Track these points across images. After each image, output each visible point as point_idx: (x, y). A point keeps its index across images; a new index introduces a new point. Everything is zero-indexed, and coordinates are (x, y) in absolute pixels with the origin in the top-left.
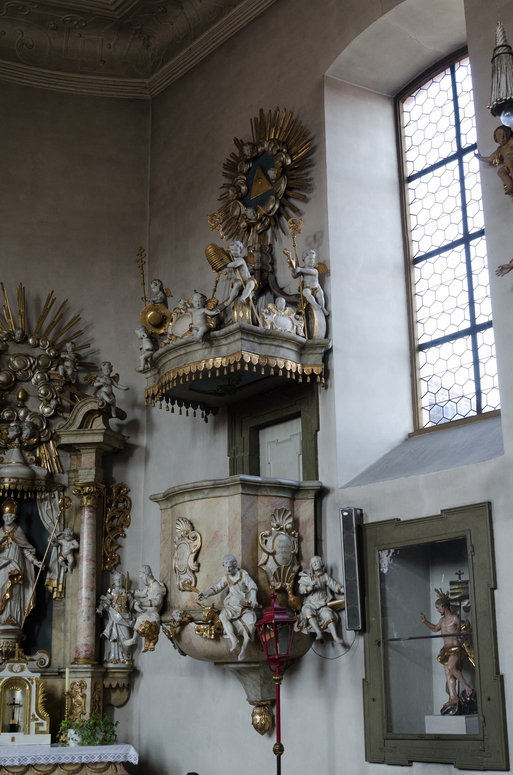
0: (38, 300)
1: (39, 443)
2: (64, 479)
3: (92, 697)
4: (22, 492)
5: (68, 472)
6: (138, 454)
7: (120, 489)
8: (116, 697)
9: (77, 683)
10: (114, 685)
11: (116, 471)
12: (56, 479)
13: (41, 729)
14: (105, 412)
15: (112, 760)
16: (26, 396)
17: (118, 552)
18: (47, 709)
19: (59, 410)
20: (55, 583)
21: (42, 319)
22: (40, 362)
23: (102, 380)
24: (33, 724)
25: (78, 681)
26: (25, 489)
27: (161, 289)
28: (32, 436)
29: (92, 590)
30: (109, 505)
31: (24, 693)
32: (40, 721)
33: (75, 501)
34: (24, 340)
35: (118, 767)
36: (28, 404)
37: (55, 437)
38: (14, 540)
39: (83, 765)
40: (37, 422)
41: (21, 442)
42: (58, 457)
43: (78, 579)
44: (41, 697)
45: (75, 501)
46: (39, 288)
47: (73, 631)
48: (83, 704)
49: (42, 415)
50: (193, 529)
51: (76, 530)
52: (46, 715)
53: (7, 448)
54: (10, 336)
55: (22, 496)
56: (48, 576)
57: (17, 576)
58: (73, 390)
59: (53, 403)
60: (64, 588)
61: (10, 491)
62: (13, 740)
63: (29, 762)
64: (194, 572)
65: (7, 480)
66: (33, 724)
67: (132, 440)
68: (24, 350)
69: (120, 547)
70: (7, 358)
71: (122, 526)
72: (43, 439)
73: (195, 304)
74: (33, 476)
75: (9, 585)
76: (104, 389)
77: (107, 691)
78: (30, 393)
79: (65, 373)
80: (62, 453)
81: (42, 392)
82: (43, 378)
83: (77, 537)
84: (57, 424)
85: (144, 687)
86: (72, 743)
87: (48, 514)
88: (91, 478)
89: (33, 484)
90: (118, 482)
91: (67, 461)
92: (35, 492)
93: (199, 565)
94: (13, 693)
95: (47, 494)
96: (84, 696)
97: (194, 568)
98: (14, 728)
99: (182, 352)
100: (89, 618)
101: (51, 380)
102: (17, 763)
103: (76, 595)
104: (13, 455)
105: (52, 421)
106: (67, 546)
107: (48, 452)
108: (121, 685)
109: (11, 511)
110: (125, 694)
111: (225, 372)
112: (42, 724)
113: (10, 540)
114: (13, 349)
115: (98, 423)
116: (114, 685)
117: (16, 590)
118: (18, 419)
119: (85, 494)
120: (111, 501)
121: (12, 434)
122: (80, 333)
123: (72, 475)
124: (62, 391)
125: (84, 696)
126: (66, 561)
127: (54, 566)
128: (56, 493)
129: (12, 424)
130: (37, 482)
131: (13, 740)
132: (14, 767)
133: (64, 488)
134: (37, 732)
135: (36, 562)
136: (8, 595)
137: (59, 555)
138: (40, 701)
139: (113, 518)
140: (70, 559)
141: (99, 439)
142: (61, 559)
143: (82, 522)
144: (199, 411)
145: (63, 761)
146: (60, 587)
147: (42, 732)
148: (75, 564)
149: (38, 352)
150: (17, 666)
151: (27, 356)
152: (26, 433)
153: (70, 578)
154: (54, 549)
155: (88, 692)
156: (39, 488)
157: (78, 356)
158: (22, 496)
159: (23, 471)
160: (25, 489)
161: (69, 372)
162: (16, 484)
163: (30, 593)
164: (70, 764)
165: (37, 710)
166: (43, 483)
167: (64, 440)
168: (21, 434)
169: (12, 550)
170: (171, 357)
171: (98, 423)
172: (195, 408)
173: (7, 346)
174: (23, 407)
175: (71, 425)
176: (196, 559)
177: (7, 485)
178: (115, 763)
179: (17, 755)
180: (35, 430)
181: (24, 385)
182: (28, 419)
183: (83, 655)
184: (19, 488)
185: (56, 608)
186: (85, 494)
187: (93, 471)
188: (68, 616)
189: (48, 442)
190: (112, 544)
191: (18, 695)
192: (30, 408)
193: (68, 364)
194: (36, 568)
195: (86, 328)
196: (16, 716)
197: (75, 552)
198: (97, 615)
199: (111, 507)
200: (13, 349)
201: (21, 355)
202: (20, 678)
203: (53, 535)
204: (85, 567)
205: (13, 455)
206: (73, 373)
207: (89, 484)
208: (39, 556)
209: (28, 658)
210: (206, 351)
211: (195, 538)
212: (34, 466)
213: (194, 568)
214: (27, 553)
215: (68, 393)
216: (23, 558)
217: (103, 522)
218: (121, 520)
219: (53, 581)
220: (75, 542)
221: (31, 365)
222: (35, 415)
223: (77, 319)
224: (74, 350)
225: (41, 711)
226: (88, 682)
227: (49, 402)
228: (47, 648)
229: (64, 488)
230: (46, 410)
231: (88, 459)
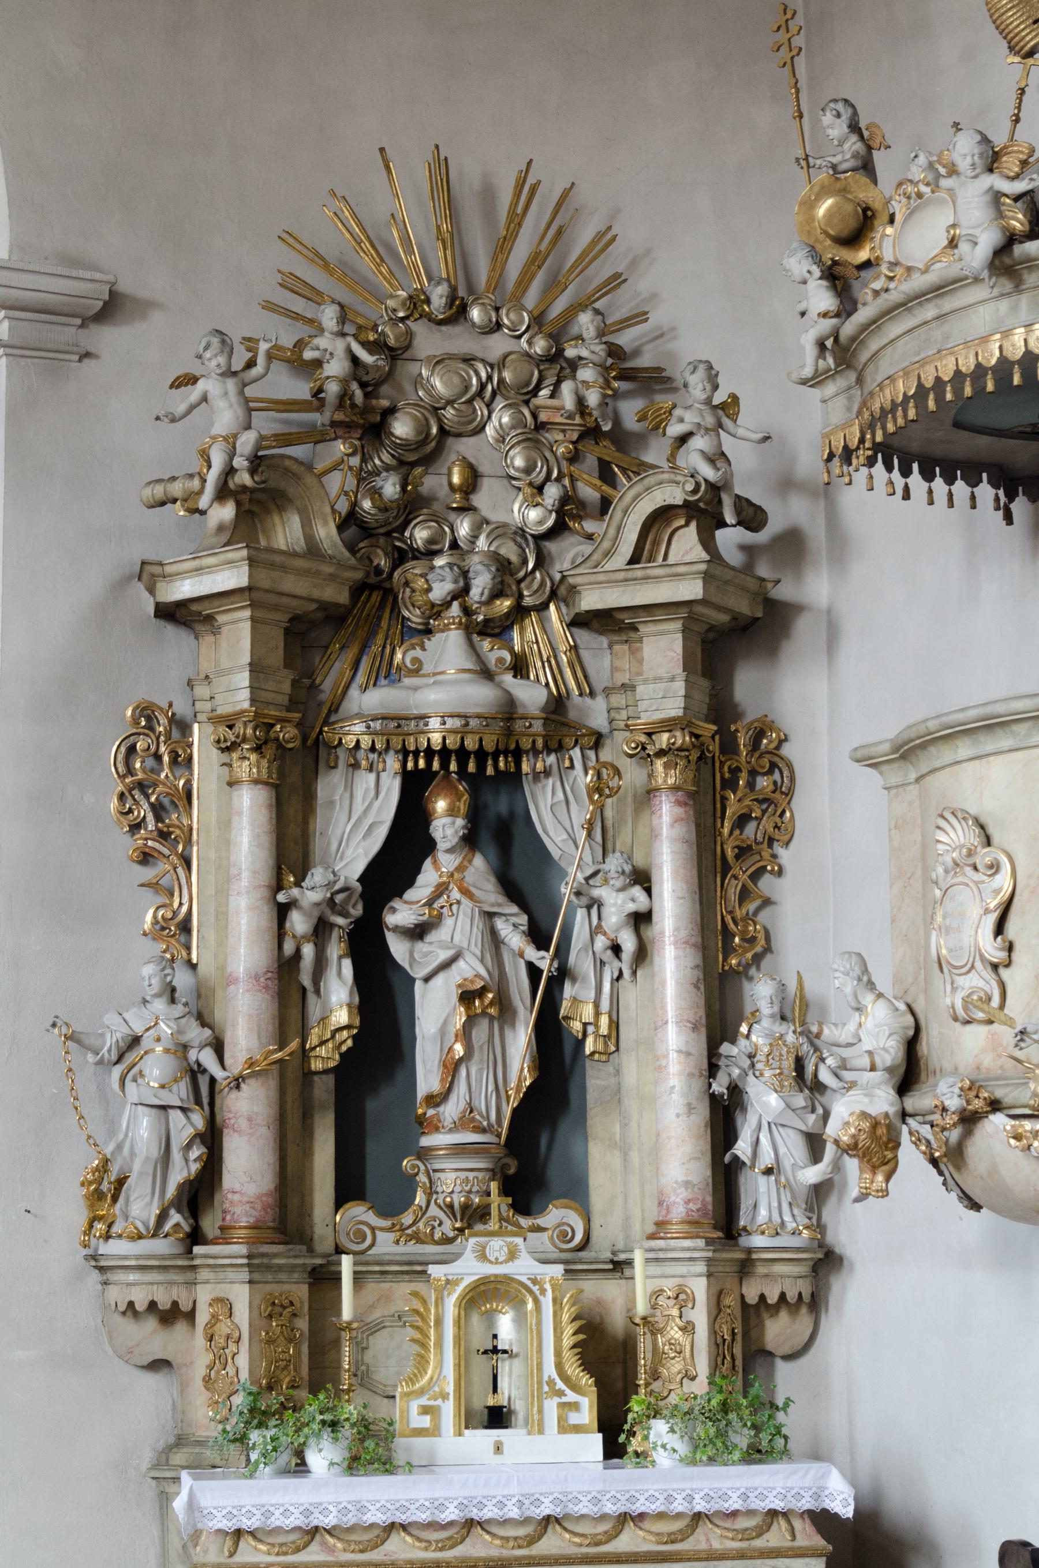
0: (488, 194)
1: (520, 612)
2: (595, 714)
3: (713, 1332)
4: (481, 755)
5: (608, 691)
6: (805, 631)
7: (760, 734)
8: (778, 1331)
9: (669, 1293)
10: (773, 1298)
11: (747, 684)
12: (572, 715)
13: (574, 1418)
14: (705, 511)
15: (779, 1505)
16: (473, 478)
17: (763, 917)
18: (587, 1365)
19: (568, 515)
20: (587, 1012)
21: (503, 247)
22: (507, 375)
23: (691, 419)
24: (551, 1407)
25: (669, 1286)
26: (489, 746)
27: (854, 127)
28: (497, 593)
29: (695, 1028)
30: (731, 784)
31: (520, 1320)
32: (571, 1396)
33: (633, 775)
34: (457, 312)
35: (797, 1524)
36: (478, 500)
37: (560, 592)
38: (465, 892)
39: (698, 1517)
40: (509, 550)
41: (467, 611)
42: (575, 648)
43: (654, 998)
44: (569, 1330)
45: (633, 775)
46: (487, 160)
47: (644, 1142)
48: (685, 1354)
49: (521, 532)
50: (988, 842)
51: (639, 860)
52: (586, 1381)
53: (428, 632)
54: (416, 303)
55: (481, 766)
56: (569, 990)
57: (481, 992)
58: (607, 450)
59: (552, 492)
60: (615, 1025)
61: (445, 753)
62: (498, 1449)
63: (547, 1509)
64: (995, 967)
65: (434, 723)
66: (551, 1407)
67: (784, 592)
68: (458, 340)
69: (767, 902)
70: (413, 368)
71: (771, 841)
72: (528, 601)
73: (964, 165)
74: (509, 711)
75: (460, 1018)
76: (699, 443)
77: (754, 1313)
78: (484, 468)
79: (581, 402)
80: (583, 636)
81: (519, 462)
82: (518, 422)
83: (642, 879)
84: (566, 553)
85: (853, 1297)
86: (662, 1459)
87: (556, 810)
88: (674, 708)
89: (509, 732)
90: (751, 715)
91: (602, 657)
92: (517, 754)
93: (1010, 948)
94: (490, 1318)
95: (552, 759)
96: (688, 1328)
97: (997, 955)
98: (497, 1418)
99: (929, 312)
100: (690, 1108)
101: (540, 427)
102: (514, 1513)
103: (650, 1044)
104: (448, 650)
105: (551, 547)
106: (618, 903)
107: (546, 634)
108: (792, 1297)
109: (452, 812)
110: (804, 1321)
111: (968, 391)
112: (575, 1406)
113: (455, 894)
114: (429, 341)
115: (686, 544)
116: (773, 1298)
117: (480, 1033)
118: (454, 545)
119: (661, 753)
120: (735, 771)
121: (440, 590)
122: (616, 281)
123: (617, 700)
124: (574, 458)
125: (688, 1328)
126: (616, 949)
127: (580, 960)
128: (576, 754)
129: (440, 562)
130: (519, 726)
131: (498, 1449)
132: (506, 1522)
133: (598, 740)
134: (565, 1427)
135: (532, 954)
136: (459, 1049)
137: (596, 931)
138: (568, 1341)
139: (742, 820)
140: (628, 942)
141: (692, 590)
142: (601, 942)
143: (654, 834)
144: (986, 492)
145: (639, 1507)
146: (604, 1021)
147: (577, 1429)
148: (642, 954)
149: (498, 345)
150: (497, 1246)
151: (468, 360)
152: (481, 583)
153: (631, 995)
154: (581, 914)
155: (700, 1316)
156: (526, 743)
157: (615, 352)
158: (481, 766)
159: (479, 696)
160: (489, 746)
161: (593, 398)
162: (463, 732)
163: (520, 1040)
164: (661, 1516)
165: (559, 1366)
166: (538, 726)
167: (590, 601)
168: (466, 590)
169: (464, 921)
170: (894, 329)
171: (686, 544)
172: (973, 482)
173: (410, 334)
174: (466, 509)
175: (608, 554)
176: (1000, 929)
177: (436, 739)
178: (785, 1515)
179: (514, 1490)
180: (503, 567)
181: (466, 447)
182: (482, 543)
183: (678, 1212)
184: (471, 744)
185: (596, 1081)
186: (661, 753)
187: (679, 687)
188: (631, 1104)
189: (545, 606)
190: (745, 895)
191: (506, 1327)
192: (486, 511)
193: (586, 374)
194: (534, 972)
195: (634, 263)
196: (503, 1383)
197: (641, 920)
198: (714, 1099)
199: (733, 781)
200: (429, 341)
201: (451, 357)
202: (507, 1279)
203: (575, 875)
204: (673, 964)
205: (448, 650)
206: (603, 404)
207: (669, 725)
208: (539, 937)
209: (525, 1222)
210: (1004, 305)
211: (995, 868)
212: (508, 679)
213: (997, 955)
214: (503, 928)
215: (591, 462)
216: (495, 941)
217: (716, 833)
218: (767, 824)
219: (582, 1006)
220: (637, 892)
221: (482, 387)
222: (501, 531)
223: (604, 240)
224: (601, 334)
225: (573, 1368)
226: (699, 1288)
227: (540, 489)
228: (577, 1192)
229: (598, 740)
230: (533, 515)
231: (663, 651)
